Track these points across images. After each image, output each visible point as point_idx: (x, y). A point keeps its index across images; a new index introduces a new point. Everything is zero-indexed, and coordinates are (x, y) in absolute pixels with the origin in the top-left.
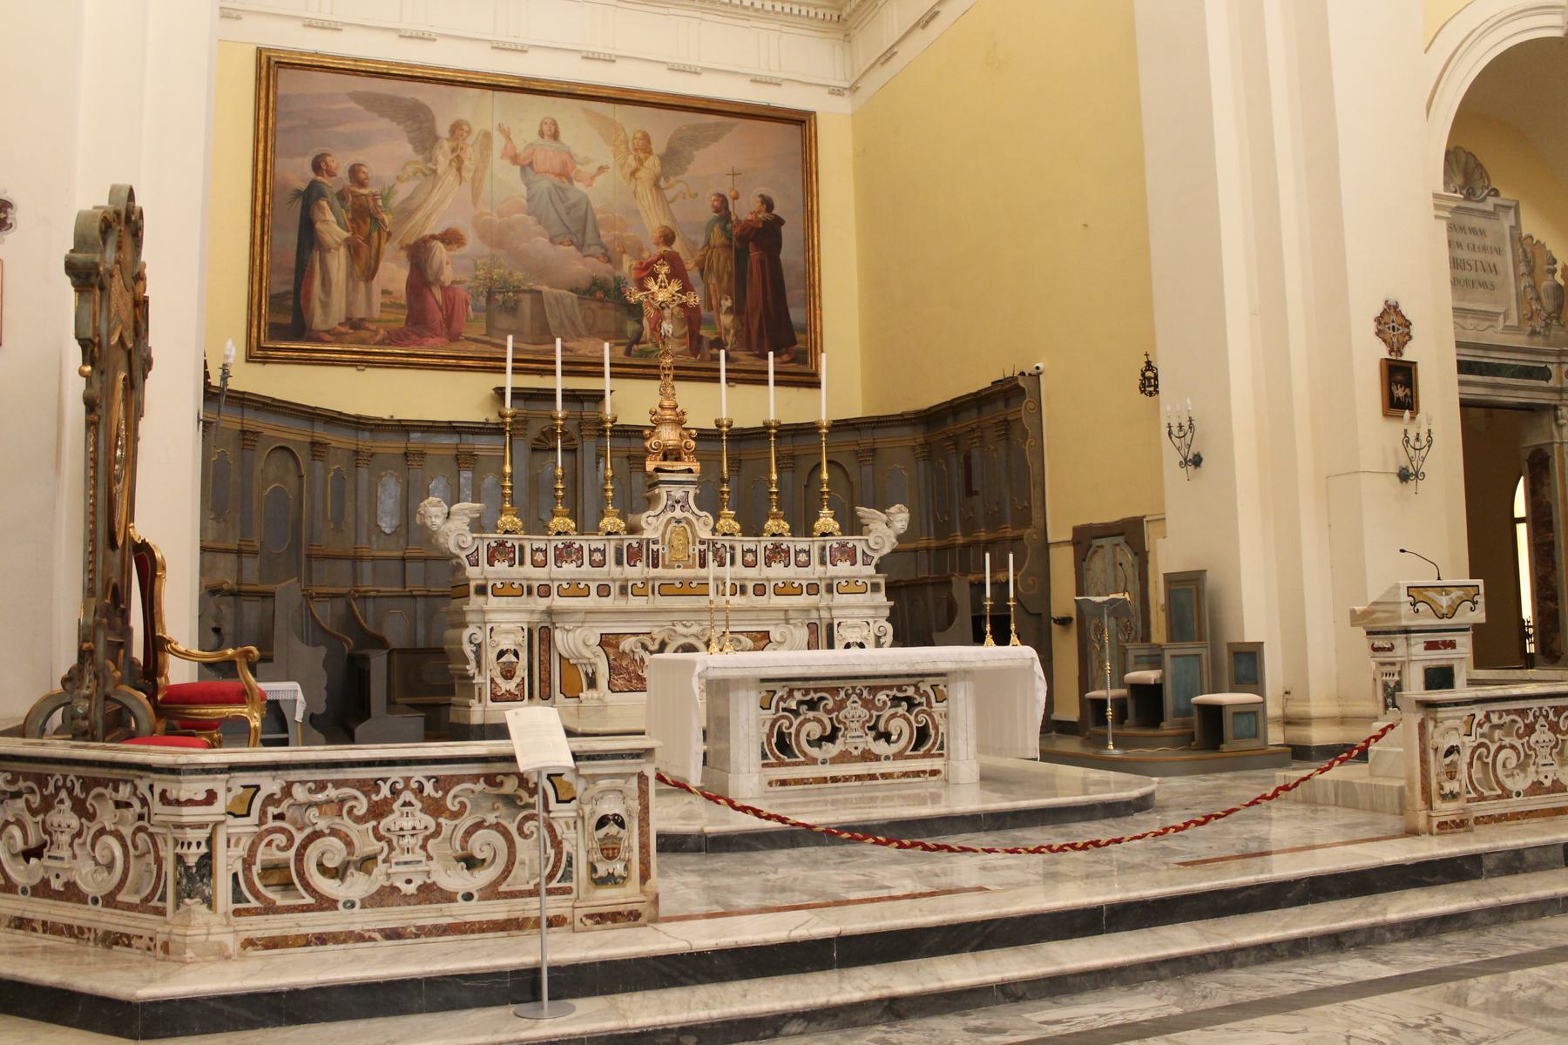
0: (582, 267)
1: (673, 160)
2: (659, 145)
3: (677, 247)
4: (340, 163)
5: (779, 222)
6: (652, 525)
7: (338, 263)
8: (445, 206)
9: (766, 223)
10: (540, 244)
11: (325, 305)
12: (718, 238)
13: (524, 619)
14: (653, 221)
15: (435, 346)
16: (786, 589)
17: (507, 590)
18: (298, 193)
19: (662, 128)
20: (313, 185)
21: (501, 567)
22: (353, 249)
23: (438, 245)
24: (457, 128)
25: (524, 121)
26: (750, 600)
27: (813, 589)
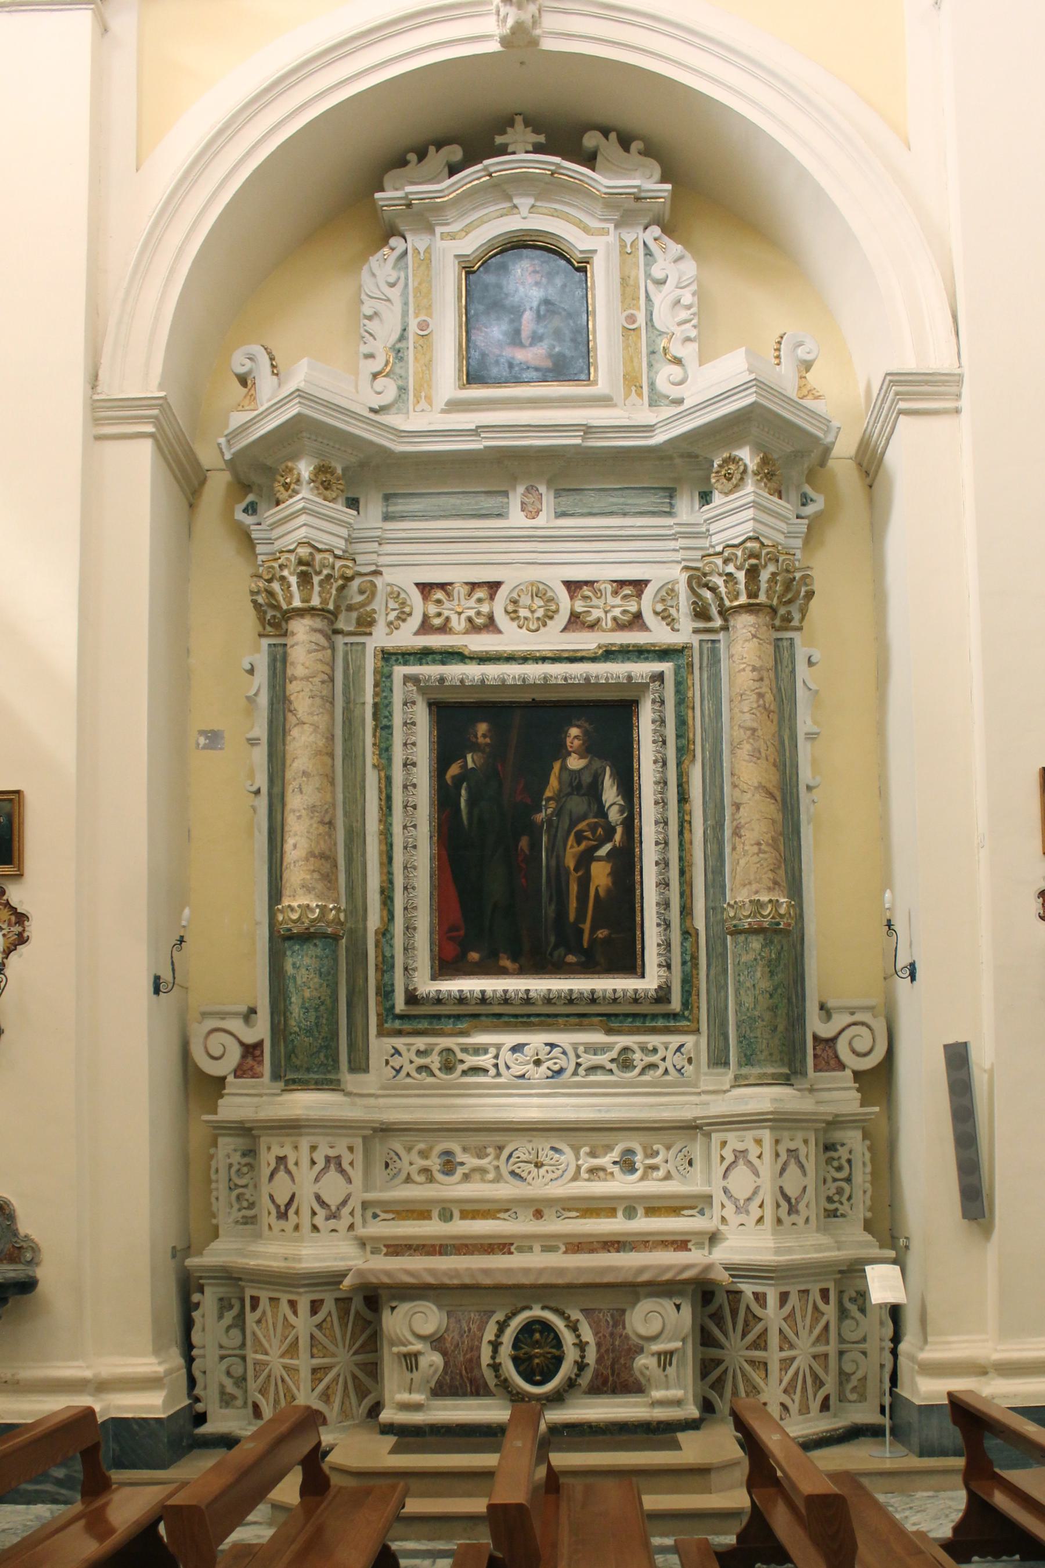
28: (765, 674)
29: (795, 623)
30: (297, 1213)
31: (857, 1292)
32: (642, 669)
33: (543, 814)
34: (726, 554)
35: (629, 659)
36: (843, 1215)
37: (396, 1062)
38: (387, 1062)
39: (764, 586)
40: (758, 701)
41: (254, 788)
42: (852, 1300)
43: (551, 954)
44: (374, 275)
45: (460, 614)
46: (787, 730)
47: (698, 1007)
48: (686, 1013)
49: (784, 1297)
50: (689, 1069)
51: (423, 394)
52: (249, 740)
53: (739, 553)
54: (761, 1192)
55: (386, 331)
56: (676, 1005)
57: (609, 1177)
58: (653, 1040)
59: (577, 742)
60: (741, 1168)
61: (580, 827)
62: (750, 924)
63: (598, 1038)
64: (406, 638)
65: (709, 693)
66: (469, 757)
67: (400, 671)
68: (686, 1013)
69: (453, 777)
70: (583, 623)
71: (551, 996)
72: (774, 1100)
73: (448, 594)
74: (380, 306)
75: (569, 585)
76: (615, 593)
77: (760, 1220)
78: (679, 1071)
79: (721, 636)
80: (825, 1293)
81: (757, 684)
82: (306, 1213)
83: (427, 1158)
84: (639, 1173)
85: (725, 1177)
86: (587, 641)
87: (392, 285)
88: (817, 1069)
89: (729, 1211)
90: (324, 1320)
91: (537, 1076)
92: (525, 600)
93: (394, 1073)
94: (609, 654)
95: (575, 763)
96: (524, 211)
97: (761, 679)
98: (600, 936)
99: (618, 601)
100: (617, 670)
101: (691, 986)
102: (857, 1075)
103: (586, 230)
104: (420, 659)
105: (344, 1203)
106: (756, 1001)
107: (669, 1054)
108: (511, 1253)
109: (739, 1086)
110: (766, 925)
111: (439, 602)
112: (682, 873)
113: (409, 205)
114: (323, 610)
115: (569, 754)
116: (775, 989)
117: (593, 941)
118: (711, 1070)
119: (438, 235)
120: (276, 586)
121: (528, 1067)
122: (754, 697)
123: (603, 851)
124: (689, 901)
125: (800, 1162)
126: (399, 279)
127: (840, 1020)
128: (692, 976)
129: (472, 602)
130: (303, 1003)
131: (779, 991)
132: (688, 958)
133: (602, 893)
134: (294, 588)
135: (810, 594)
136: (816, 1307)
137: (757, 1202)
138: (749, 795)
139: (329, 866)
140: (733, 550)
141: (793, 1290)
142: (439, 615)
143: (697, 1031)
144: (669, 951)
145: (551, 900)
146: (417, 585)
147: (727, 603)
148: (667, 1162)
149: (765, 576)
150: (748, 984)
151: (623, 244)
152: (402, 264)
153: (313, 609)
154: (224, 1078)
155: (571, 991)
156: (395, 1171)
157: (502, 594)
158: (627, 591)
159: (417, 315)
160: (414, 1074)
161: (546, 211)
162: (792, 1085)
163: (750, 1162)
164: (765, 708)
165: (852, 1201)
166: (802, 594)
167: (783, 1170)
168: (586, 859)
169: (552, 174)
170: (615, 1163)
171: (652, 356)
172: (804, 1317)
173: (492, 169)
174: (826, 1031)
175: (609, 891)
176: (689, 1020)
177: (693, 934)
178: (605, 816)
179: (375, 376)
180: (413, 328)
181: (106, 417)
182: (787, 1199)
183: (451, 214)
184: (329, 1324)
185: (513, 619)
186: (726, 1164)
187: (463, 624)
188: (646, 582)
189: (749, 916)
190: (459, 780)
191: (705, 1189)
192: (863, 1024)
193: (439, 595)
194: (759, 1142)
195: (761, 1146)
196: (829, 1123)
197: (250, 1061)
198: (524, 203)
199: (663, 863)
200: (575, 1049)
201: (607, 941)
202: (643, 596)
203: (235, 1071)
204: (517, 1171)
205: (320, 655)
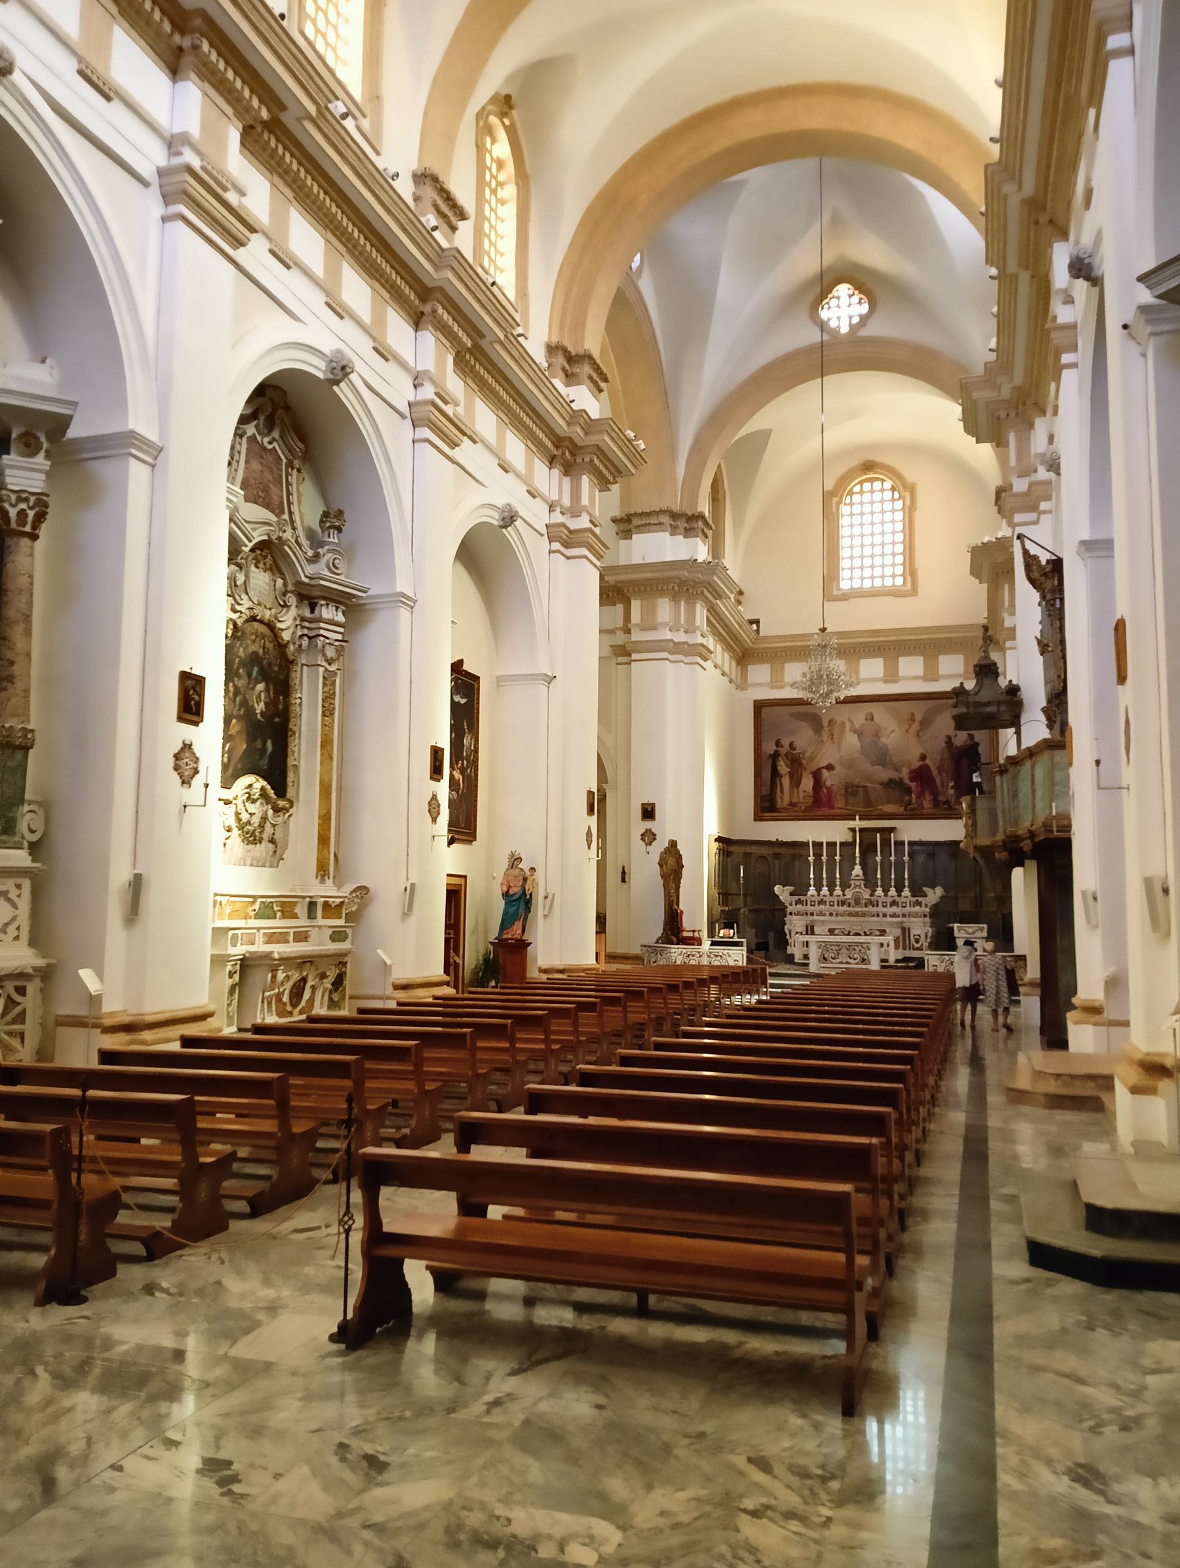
0: (886, 774)
1: (925, 723)
2: (918, 717)
3: (927, 761)
4: (785, 742)
5: (978, 744)
6: (849, 894)
7: (786, 781)
8: (828, 754)
9: (971, 746)
10: (866, 766)
11: (782, 798)
12: (947, 755)
13: (804, 923)
14: (915, 751)
15: (825, 811)
16: (894, 915)
17: (798, 914)
18: (771, 756)
19: (919, 709)
20: (776, 751)
21: (799, 906)
22: (791, 774)
23: (824, 771)
24: (830, 721)
25: (858, 716)
26: (881, 918)
27: (904, 915)
77: (17, 938)
137: (14, 925)
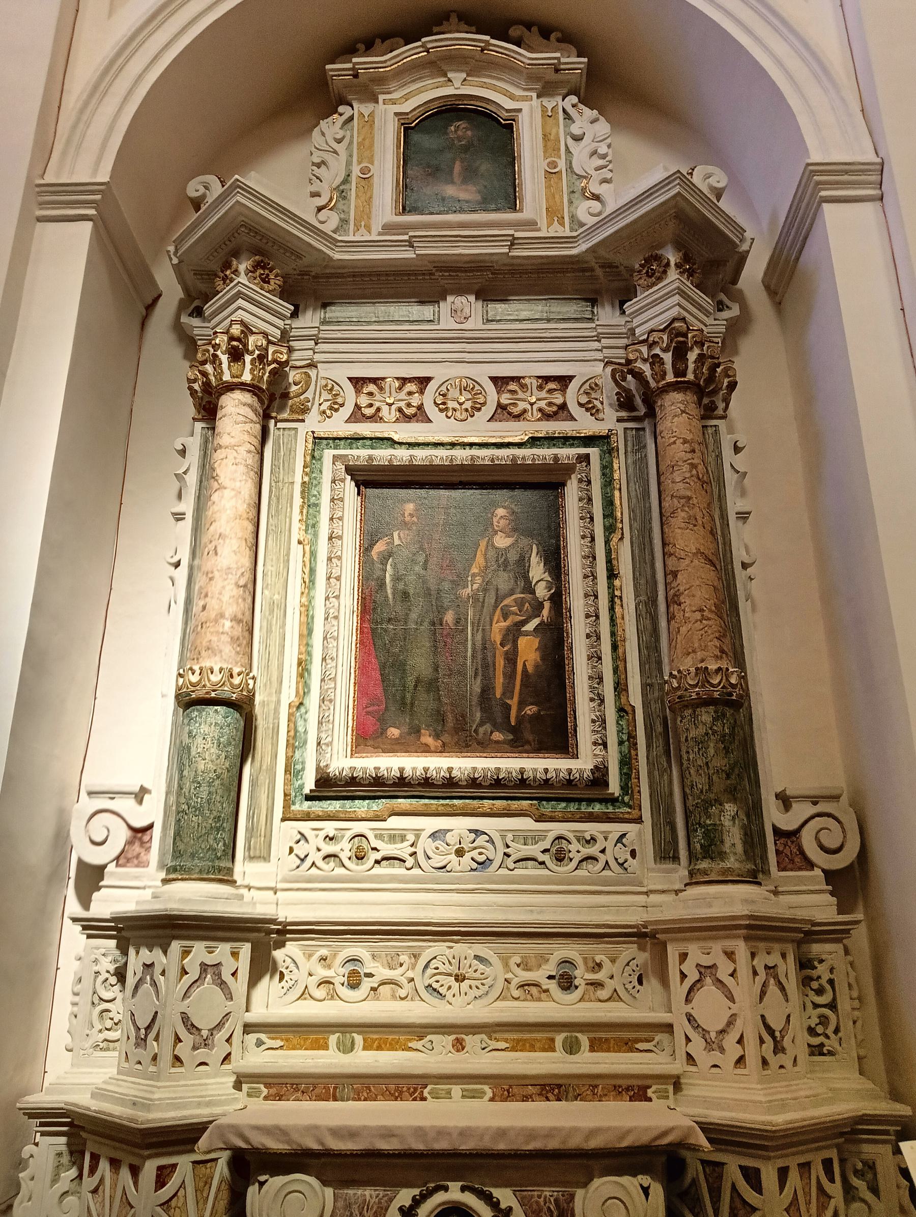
28: (696, 447)
29: (720, 412)
30: (157, 1039)
31: (865, 1163)
32: (567, 453)
33: (469, 590)
34: (651, 339)
35: (554, 445)
36: (830, 1053)
37: (301, 849)
38: (291, 850)
39: (691, 366)
40: (691, 471)
41: (175, 560)
42: (858, 1173)
43: (476, 731)
44: (323, 134)
45: (390, 405)
46: (717, 510)
47: (639, 792)
48: (626, 799)
49: (783, 1173)
50: (632, 863)
51: (363, 224)
52: (174, 514)
53: (665, 337)
54: (739, 1022)
55: (333, 175)
56: (614, 787)
57: (543, 995)
58: (591, 828)
59: (502, 522)
60: (709, 989)
61: (506, 602)
62: (698, 694)
63: (526, 823)
64: (338, 425)
65: (635, 475)
66: (396, 534)
67: (328, 454)
68: (626, 799)
69: (379, 553)
70: (510, 414)
71: (476, 776)
72: (746, 901)
73: (381, 389)
74: (328, 157)
75: (494, 380)
76: (540, 388)
77: (741, 1061)
78: (621, 865)
79: (646, 424)
80: (827, 1164)
81: (689, 456)
82: (167, 1038)
83: (329, 967)
84: (578, 994)
85: (688, 1000)
86: (516, 432)
87: (339, 141)
88: (781, 868)
89: (697, 1047)
90: (175, 1195)
91: (459, 868)
92: (454, 393)
93: (298, 862)
94: (534, 441)
95: (502, 541)
96: (457, 83)
97: (693, 451)
98: (529, 712)
99: (543, 394)
100: (545, 453)
101: (630, 769)
102: (830, 876)
103: (512, 97)
104: (351, 444)
105: (220, 1025)
106: (711, 783)
107: (609, 845)
108: (424, 1099)
109: (697, 883)
110: (716, 695)
111: (371, 394)
112: (615, 647)
113: (356, 76)
114: (253, 386)
115: (496, 533)
116: (732, 769)
117: (520, 719)
118: (658, 866)
119: (381, 101)
120: (209, 368)
121: (449, 857)
122: (686, 468)
123: (531, 626)
124: (623, 676)
125: (780, 983)
126: (344, 137)
127: (801, 811)
128: (630, 758)
129: (403, 395)
130: (196, 775)
131: (736, 771)
132: (625, 737)
133: (530, 669)
134: (225, 365)
135: (732, 386)
136: (821, 1189)
137: (733, 1036)
138: (687, 562)
139: (240, 630)
140: (660, 334)
141: (792, 1163)
142: (371, 405)
143: (639, 820)
144: (605, 728)
145: (476, 674)
146: (350, 379)
147: (653, 384)
148: (612, 977)
149: (692, 356)
150: (699, 762)
151: (544, 109)
152: (349, 125)
153: (242, 384)
154: (104, 867)
155: (498, 769)
156: (291, 983)
157: (432, 387)
158: (552, 385)
159: (359, 163)
160: (320, 863)
161: (475, 83)
162: (759, 884)
163: (721, 982)
164: (699, 479)
165: (840, 1034)
166: (725, 384)
167: (763, 993)
168: (513, 633)
169: (482, 51)
170: (551, 977)
171: (572, 195)
172: (808, 1203)
173: (429, 46)
174: (788, 822)
175: (537, 666)
176: (630, 807)
177: (630, 712)
178: (533, 592)
179: (320, 209)
180: (356, 171)
181: (51, 200)
182: (771, 1031)
183: (393, 85)
184: (182, 1200)
185: (441, 410)
186: (688, 983)
187: (394, 414)
188: (571, 378)
189: (696, 686)
190: (385, 557)
191: (662, 1016)
192: (829, 815)
193: (372, 388)
194: (730, 955)
195: (734, 961)
196: (808, 933)
197: (137, 848)
198: (458, 77)
199: (594, 636)
200: (503, 837)
201: (536, 717)
202: (568, 391)
203: (117, 858)
204: (435, 985)
205: (248, 427)
